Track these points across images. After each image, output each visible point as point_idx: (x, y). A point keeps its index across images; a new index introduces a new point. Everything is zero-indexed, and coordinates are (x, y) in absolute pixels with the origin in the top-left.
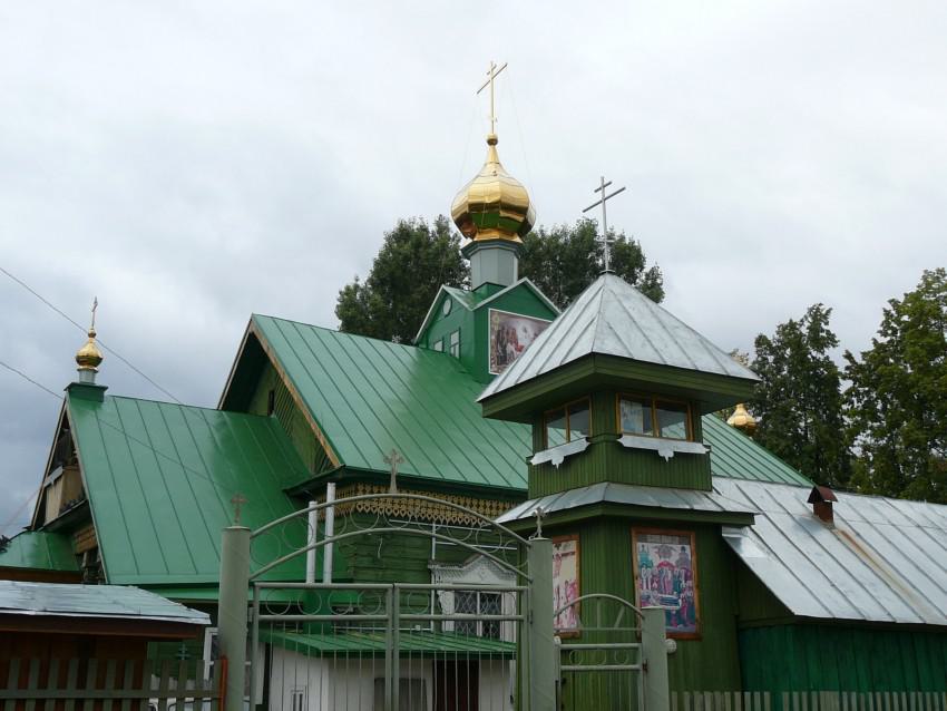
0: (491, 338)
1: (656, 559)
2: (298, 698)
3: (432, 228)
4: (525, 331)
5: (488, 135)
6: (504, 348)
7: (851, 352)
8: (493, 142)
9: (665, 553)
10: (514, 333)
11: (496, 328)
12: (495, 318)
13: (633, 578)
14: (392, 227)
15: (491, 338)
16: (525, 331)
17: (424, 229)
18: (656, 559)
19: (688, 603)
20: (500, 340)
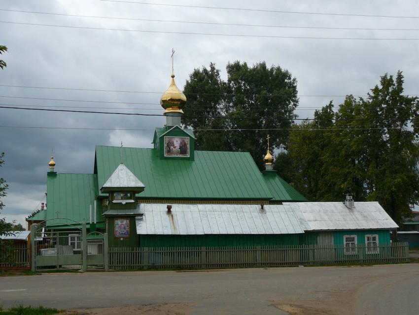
0: (165, 145)
1: (120, 223)
2: (135, 263)
3: (209, 69)
4: (177, 141)
5: (171, 74)
6: (170, 149)
7: (341, 104)
8: (173, 77)
9: (123, 222)
10: (173, 143)
11: (167, 142)
12: (166, 139)
13: (114, 227)
14: (192, 72)
15: (165, 145)
16: (177, 141)
17: (205, 70)
18: (120, 223)
19: (127, 231)
20: (168, 146)
